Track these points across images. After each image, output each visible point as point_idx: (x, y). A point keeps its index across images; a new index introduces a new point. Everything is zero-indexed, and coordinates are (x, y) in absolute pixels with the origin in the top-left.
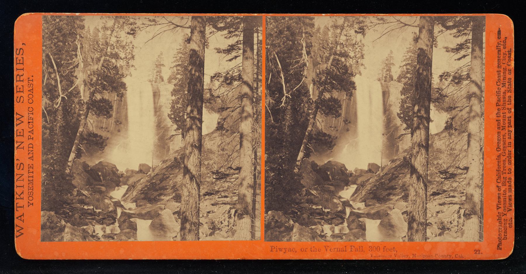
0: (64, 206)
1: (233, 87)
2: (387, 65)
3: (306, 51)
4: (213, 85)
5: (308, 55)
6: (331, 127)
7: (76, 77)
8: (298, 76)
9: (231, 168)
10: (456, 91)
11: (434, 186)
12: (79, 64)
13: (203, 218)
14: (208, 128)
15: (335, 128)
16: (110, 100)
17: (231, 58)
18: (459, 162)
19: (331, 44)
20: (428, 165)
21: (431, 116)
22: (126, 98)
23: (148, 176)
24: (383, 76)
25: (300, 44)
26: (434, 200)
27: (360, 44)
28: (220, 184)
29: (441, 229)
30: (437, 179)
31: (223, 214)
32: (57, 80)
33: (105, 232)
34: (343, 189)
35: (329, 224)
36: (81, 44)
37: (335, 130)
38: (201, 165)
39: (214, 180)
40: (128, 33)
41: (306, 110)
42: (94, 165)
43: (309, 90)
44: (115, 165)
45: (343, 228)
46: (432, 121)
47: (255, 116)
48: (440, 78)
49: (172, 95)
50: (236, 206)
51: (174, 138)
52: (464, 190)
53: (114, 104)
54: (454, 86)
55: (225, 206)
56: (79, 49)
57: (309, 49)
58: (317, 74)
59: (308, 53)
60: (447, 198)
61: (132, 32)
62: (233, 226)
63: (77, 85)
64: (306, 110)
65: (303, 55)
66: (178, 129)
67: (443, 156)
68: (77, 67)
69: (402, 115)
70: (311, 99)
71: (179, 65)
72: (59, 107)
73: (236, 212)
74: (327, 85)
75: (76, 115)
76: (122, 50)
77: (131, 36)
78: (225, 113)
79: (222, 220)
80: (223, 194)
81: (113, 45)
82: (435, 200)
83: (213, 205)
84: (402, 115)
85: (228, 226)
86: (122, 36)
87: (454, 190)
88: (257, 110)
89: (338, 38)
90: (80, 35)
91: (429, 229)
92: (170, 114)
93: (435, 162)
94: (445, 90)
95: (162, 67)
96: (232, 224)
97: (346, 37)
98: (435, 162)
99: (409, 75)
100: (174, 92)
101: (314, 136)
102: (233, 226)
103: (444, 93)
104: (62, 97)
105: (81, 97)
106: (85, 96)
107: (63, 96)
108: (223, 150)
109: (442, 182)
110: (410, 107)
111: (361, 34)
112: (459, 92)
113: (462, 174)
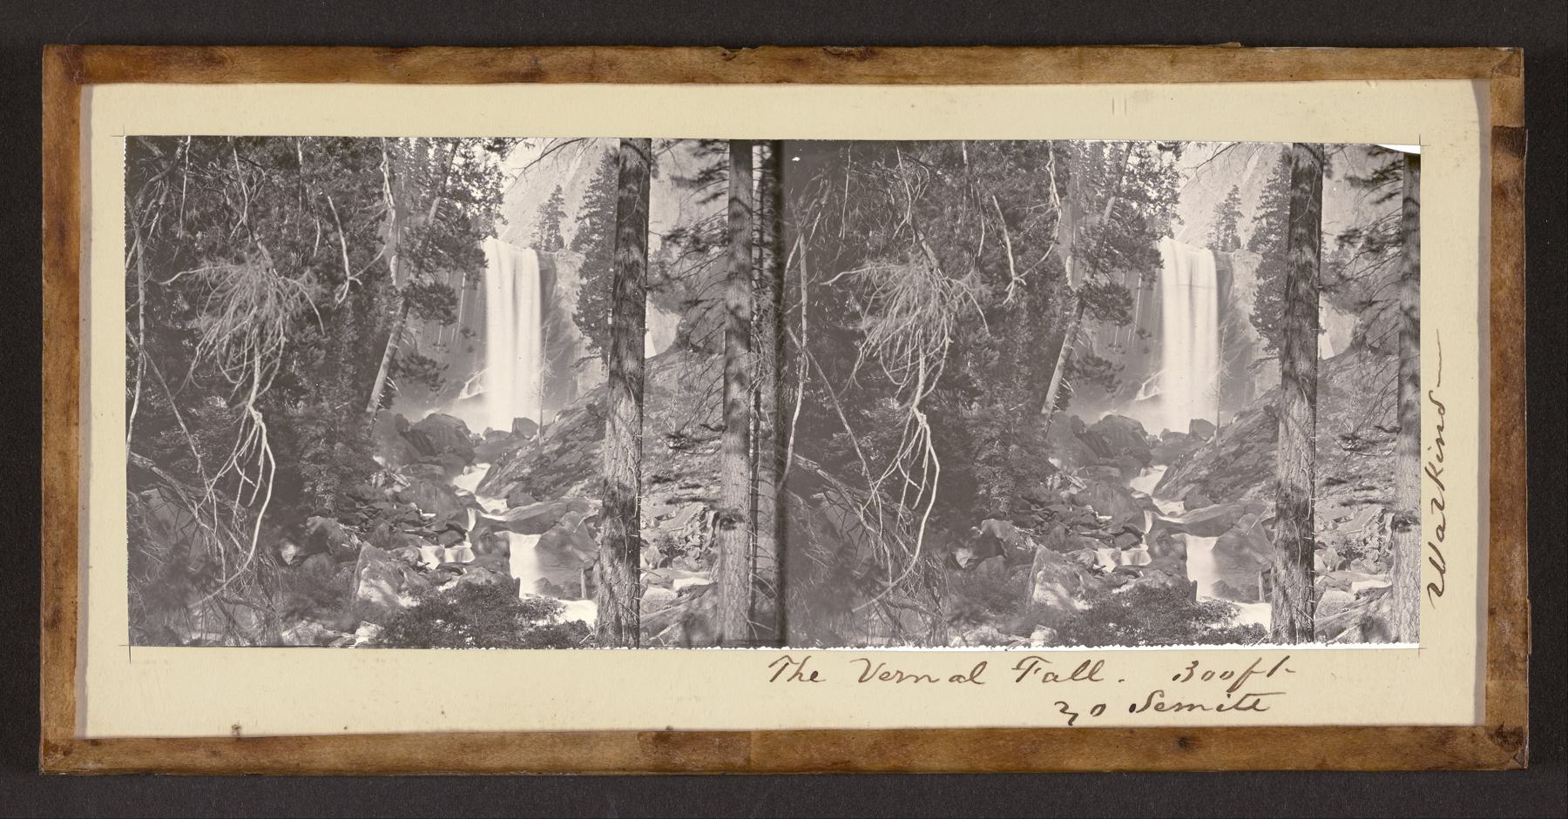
0: (1033, 508)
1: (708, 259)
2: (550, 216)
3: (1057, 187)
4: (668, 255)
5: (1061, 197)
6: (1110, 346)
7: (380, 239)
8: (1041, 239)
9: (706, 426)
10: (1372, 269)
11: (1330, 466)
12: (385, 212)
13: (648, 530)
14: (656, 343)
15: (1120, 346)
16: (451, 286)
17: (1379, 198)
18: (1381, 417)
19: (1109, 173)
20: (1315, 422)
21: (1321, 321)
22: (484, 284)
23: (530, 443)
24: (542, 238)
25: (1043, 173)
26: (1328, 495)
27: (1169, 173)
28: (684, 460)
29: (1345, 556)
30: (1335, 452)
31: (1367, 525)
32: (341, 246)
33: (1118, 562)
34: (1138, 475)
35: (434, 544)
36: (392, 172)
37: (1120, 350)
38: (642, 421)
39: (671, 451)
40: (490, 148)
41: (383, 310)
42: (1096, 422)
43: (389, 269)
44: (1140, 424)
45: (462, 551)
46: (1324, 332)
47: (755, 318)
48: (1338, 242)
49: (581, 278)
50: (716, 505)
51: (1262, 366)
52: (1392, 473)
53: (460, 294)
54: (1367, 259)
55: (696, 504)
56: (386, 183)
57: (1063, 183)
58: (407, 236)
59: (1062, 192)
60: (1355, 490)
61: (497, 146)
62: (711, 546)
63: (382, 256)
64: (383, 310)
65: (1052, 197)
66: (1270, 347)
67: (1347, 405)
68: (383, 220)
69: (583, 319)
70: (394, 287)
71: (595, 214)
72: (344, 302)
73: (716, 517)
74: (1103, 257)
75: (381, 319)
76: (477, 184)
77: (495, 154)
78: (694, 313)
79: (1366, 535)
80: (689, 481)
81: (458, 172)
82: (654, 492)
83: (669, 502)
84: (583, 319)
85: (701, 546)
86: (476, 154)
87: (1372, 476)
88: (759, 306)
89: (1124, 160)
90: (389, 153)
91: (1320, 555)
92: (576, 313)
93: (1331, 417)
94: (1350, 268)
95: (1236, 219)
96: (708, 543)
97: (1139, 159)
98: (1331, 417)
99: (1272, 237)
100: (1262, 272)
101: (1075, 364)
102: (711, 546)
103: (1347, 273)
104: (351, 281)
105: (1066, 280)
106: (1074, 274)
107: (352, 278)
108: (690, 388)
109: (1345, 459)
110: (1276, 302)
111: (1171, 153)
112: (1379, 270)
113: (1387, 441)
